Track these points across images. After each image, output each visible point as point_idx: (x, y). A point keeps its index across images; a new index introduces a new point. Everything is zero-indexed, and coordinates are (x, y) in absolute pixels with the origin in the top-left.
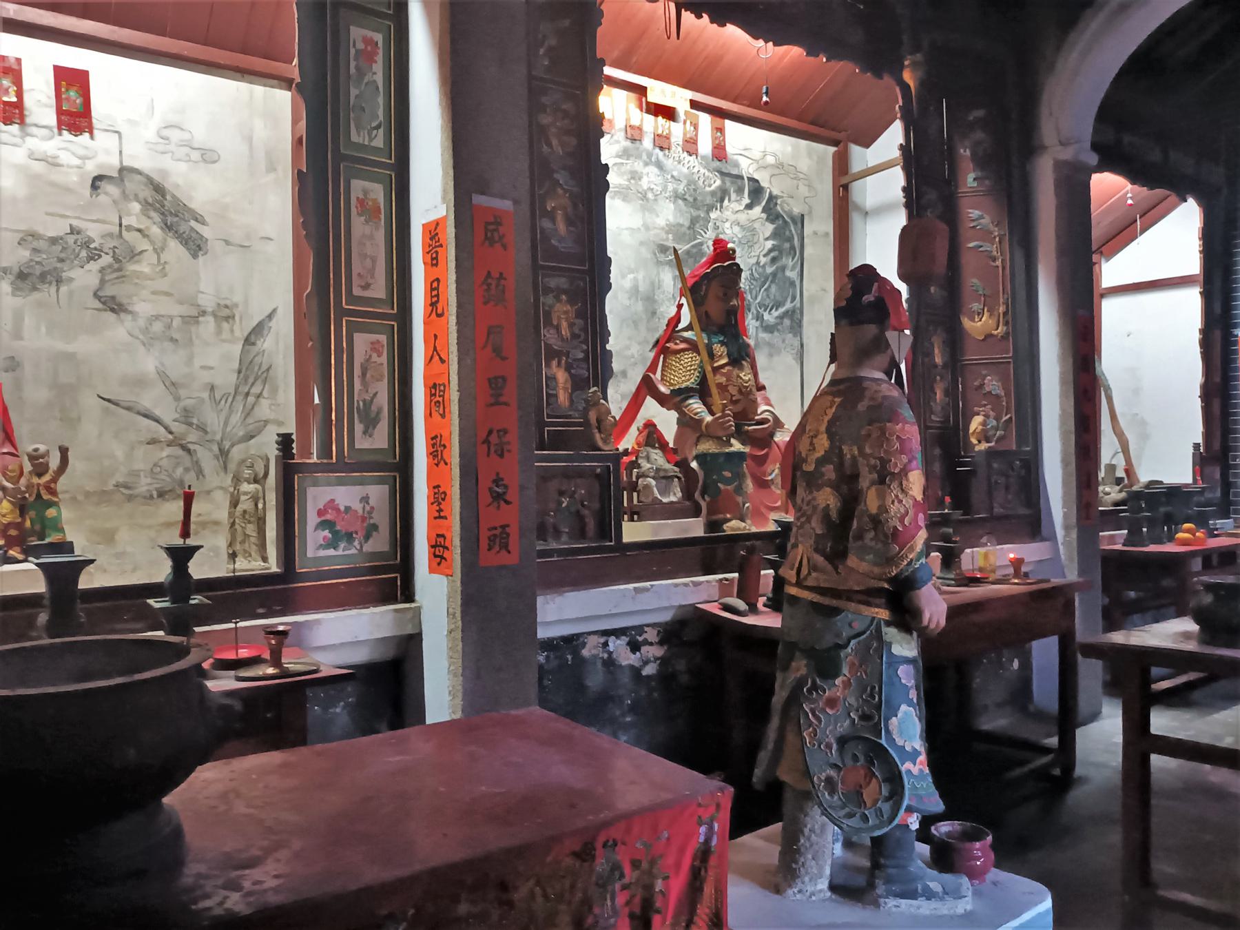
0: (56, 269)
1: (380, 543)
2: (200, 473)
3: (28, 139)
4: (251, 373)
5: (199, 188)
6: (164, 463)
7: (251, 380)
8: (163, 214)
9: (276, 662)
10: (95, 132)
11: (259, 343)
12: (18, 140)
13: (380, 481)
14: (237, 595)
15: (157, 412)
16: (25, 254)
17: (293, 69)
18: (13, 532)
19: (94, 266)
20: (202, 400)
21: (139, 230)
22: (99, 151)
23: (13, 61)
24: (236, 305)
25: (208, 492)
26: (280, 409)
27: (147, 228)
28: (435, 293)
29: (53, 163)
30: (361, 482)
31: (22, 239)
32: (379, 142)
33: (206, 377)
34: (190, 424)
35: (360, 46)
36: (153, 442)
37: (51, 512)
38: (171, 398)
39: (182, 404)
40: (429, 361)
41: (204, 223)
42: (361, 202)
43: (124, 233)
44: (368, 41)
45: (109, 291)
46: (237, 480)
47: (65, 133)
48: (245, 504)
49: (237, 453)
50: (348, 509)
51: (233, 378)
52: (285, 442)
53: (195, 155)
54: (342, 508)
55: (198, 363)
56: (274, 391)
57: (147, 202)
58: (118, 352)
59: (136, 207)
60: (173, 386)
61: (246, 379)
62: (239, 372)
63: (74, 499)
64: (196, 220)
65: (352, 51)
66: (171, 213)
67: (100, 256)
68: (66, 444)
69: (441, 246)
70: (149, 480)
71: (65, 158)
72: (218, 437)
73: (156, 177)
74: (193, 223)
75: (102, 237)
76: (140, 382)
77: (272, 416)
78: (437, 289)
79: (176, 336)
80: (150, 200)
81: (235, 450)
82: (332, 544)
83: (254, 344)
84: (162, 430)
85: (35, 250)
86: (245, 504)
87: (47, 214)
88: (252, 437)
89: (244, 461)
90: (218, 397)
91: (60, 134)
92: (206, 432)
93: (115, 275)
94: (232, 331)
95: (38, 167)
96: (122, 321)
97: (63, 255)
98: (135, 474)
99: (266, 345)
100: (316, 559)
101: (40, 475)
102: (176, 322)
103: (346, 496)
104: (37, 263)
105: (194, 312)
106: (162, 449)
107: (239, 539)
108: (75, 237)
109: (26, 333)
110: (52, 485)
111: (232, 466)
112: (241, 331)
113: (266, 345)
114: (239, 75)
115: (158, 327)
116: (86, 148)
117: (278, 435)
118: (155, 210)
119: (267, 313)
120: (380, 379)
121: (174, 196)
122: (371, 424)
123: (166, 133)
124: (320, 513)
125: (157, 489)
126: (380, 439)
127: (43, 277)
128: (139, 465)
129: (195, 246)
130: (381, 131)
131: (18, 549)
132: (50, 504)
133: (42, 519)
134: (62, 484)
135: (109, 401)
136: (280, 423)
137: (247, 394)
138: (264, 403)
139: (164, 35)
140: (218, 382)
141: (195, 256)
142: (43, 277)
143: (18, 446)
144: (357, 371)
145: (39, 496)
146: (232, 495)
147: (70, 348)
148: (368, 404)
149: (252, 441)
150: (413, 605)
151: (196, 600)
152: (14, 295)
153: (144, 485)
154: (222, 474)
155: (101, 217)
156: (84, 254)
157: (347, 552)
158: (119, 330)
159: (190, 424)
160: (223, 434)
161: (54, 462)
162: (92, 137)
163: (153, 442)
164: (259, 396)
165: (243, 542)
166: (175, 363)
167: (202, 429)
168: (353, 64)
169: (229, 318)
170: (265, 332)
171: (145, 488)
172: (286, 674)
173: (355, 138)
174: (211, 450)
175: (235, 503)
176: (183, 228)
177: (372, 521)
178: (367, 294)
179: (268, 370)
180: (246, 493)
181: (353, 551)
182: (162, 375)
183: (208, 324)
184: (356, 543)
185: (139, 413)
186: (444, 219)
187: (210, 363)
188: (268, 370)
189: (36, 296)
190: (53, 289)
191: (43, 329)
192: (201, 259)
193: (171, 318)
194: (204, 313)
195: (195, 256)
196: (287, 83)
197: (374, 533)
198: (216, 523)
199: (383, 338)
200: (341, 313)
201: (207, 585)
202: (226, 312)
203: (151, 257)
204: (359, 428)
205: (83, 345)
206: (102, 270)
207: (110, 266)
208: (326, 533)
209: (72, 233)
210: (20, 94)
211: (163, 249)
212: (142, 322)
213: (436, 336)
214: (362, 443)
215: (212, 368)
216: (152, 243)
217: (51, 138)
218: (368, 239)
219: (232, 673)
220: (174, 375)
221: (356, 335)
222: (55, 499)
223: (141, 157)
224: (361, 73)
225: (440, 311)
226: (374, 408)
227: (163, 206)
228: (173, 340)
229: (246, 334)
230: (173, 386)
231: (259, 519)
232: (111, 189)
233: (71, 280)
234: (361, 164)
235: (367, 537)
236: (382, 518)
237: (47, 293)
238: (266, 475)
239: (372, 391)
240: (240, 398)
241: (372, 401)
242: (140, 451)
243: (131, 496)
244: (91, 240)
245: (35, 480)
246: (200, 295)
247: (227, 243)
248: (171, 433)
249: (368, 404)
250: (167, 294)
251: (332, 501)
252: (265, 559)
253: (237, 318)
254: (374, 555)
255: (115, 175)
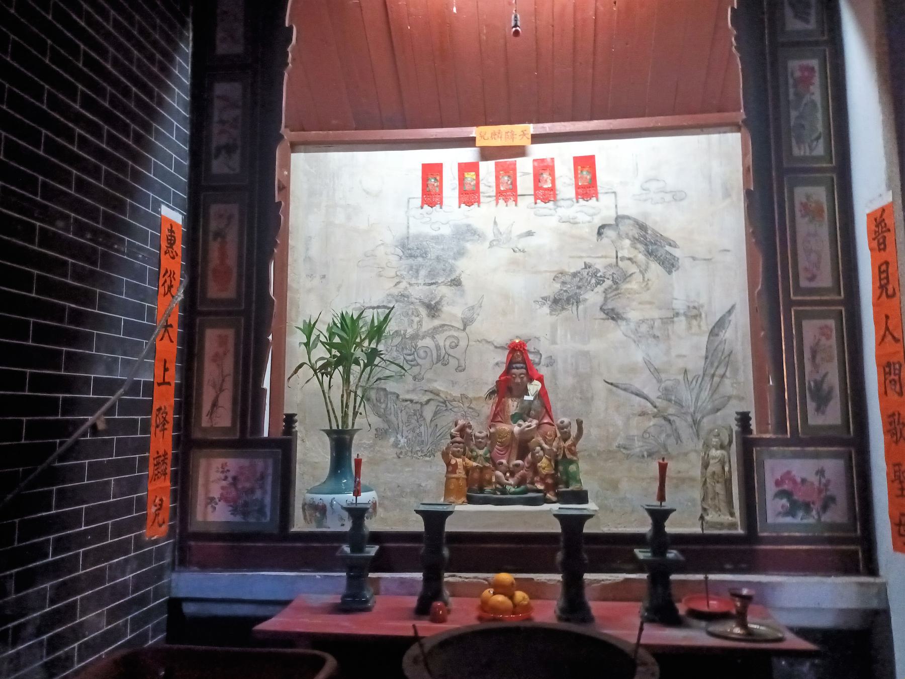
0: (576, 294)
1: (837, 515)
2: (678, 438)
3: (559, 210)
4: (716, 357)
5: (669, 221)
6: (652, 430)
7: (716, 364)
8: (646, 245)
9: (743, 625)
10: (600, 196)
11: (721, 334)
12: (553, 212)
13: (835, 455)
14: (706, 551)
15: (646, 391)
16: (557, 286)
17: (742, 115)
18: (549, 481)
19: (600, 289)
20: (679, 381)
21: (630, 259)
22: (602, 208)
23: (549, 160)
24: (702, 306)
25: (686, 454)
26: (741, 390)
27: (635, 256)
28: (883, 276)
29: (574, 223)
30: (817, 456)
31: (556, 277)
32: (820, 149)
33: (681, 363)
34: (670, 400)
35: (798, 74)
36: (643, 414)
37: (572, 468)
38: (655, 381)
39: (663, 385)
40: (881, 342)
41: (675, 246)
42: (804, 206)
43: (620, 263)
44: (804, 69)
45: (610, 306)
46: (707, 446)
47: (581, 200)
48: (714, 467)
49: (706, 423)
50: (804, 481)
51: (701, 363)
52: (744, 419)
53: (668, 197)
54: (799, 480)
55: (674, 353)
56: (736, 371)
57: (634, 238)
58: (617, 349)
59: (627, 242)
60: (656, 372)
61: (712, 364)
62: (706, 358)
63: (590, 456)
64: (670, 245)
65: (791, 81)
66: (653, 245)
67: (604, 281)
68: (581, 418)
69: (889, 230)
70: (641, 444)
71: (582, 218)
72: (692, 410)
73: (641, 219)
74: (668, 248)
75: (605, 268)
76: (633, 370)
77: (735, 393)
78: (887, 271)
79: (658, 333)
80: (637, 236)
81: (705, 420)
82: (791, 512)
83: (717, 335)
84: (649, 404)
85: (564, 283)
86: (714, 467)
87: (571, 257)
88: (718, 410)
89: (711, 431)
90: (690, 379)
91: (578, 202)
92: (682, 407)
93: (614, 293)
94: (699, 326)
95: (565, 227)
96: (619, 326)
97: (580, 284)
98: (630, 438)
99: (727, 335)
100: (775, 526)
101: (565, 440)
102: (657, 323)
103: (803, 468)
104: (566, 291)
105: (670, 314)
106: (650, 420)
107: (710, 496)
108: (587, 271)
109: (559, 341)
110: (573, 448)
111: (703, 433)
112: (706, 326)
113: (727, 335)
114: (699, 130)
115: (644, 328)
116: (594, 208)
117: (737, 413)
118: (641, 242)
119: (727, 309)
120: (830, 360)
121: (653, 230)
122: (822, 400)
123: (647, 186)
124: (778, 483)
125: (647, 450)
126: (832, 416)
127: (568, 301)
128: (634, 432)
129: (670, 264)
130: (821, 141)
131: (551, 492)
132: (572, 462)
133: (566, 472)
134: (580, 445)
135: (612, 384)
136: (741, 399)
137: (713, 376)
138: (727, 382)
139: (643, 116)
140: (690, 366)
141: (670, 272)
142: (568, 301)
143: (554, 417)
144: (807, 355)
145: (564, 456)
146: (703, 458)
147: (586, 348)
148: (819, 385)
149: (719, 414)
150: (878, 580)
151: (672, 554)
152: (551, 314)
153: (638, 447)
154: (695, 440)
155: (604, 254)
156: (593, 281)
157: (805, 521)
158: (617, 333)
159: (670, 400)
160: (696, 407)
161: (574, 431)
162: (597, 200)
163: (643, 414)
164: (723, 376)
165: (713, 499)
166: (657, 354)
167: (679, 403)
168: (791, 91)
169: (697, 316)
170: (726, 325)
171: (638, 450)
172: (750, 635)
173: (797, 152)
174: (686, 421)
175: (706, 465)
176: (661, 252)
177: (828, 493)
178: (813, 285)
179: (729, 355)
180: (714, 458)
181: (811, 521)
182: (648, 363)
183: (681, 324)
184: (814, 513)
185: (632, 393)
186: (891, 205)
187: (684, 352)
188: (729, 355)
189: (565, 313)
190: (574, 308)
191: (569, 336)
192: (674, 274)
193: (653, 320)
194: (677, 314)
195: (670, 272)
196: (735, 127)
197: (833, 506)
198: (692, 479)
199: (831, 323)
200: (790, 304)
201: (680, 540)
202: (694, 312)
203: (638, 277)
204: (811, 406)
205: (594, 346)
206: (605, 291)
207: (610, 287)
208: (784, 501)
209: (586, 268)
210: (553, 182)
211: (646, 270)
212: (632, 326)
213: (887, 317)
214: (815, 420)
215: (685, 356)
216: (639, 266)
217: (572, 205)
218: (813, 239)
219: (703, 624)
220: (657, 363)
221: (805, 323)
222: (575, 458)
223: (630, 208)
224: (799, 96)
225: (890, 292)
226: (825, 387)
227: (646, 239)
228: (655, 337)
229: (710, 327)
230: (656, 372)
231: (726, 481)
232: (610, 233)
233: (585, 300)
234: (804, 172)
235: (825, 508)
236: (839, 491)
237: (571, 311)
238: (730, 442)
239: (822, 372)
240: (707, 379)
241: (822, 381)
242: (635, 421)
243: (628, 455)
244: (598, 271)
245: (562, 444)
246: (675, 301)
247: (694, 259)
248: (655, 407)
249: (819, 385)
250: (650, 303)
251: (789, 473)
252: (732, 514)
253: (703, 315)
254: (832, 526)
255: (613, 222)
